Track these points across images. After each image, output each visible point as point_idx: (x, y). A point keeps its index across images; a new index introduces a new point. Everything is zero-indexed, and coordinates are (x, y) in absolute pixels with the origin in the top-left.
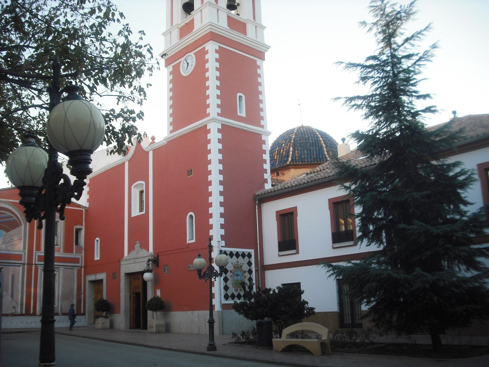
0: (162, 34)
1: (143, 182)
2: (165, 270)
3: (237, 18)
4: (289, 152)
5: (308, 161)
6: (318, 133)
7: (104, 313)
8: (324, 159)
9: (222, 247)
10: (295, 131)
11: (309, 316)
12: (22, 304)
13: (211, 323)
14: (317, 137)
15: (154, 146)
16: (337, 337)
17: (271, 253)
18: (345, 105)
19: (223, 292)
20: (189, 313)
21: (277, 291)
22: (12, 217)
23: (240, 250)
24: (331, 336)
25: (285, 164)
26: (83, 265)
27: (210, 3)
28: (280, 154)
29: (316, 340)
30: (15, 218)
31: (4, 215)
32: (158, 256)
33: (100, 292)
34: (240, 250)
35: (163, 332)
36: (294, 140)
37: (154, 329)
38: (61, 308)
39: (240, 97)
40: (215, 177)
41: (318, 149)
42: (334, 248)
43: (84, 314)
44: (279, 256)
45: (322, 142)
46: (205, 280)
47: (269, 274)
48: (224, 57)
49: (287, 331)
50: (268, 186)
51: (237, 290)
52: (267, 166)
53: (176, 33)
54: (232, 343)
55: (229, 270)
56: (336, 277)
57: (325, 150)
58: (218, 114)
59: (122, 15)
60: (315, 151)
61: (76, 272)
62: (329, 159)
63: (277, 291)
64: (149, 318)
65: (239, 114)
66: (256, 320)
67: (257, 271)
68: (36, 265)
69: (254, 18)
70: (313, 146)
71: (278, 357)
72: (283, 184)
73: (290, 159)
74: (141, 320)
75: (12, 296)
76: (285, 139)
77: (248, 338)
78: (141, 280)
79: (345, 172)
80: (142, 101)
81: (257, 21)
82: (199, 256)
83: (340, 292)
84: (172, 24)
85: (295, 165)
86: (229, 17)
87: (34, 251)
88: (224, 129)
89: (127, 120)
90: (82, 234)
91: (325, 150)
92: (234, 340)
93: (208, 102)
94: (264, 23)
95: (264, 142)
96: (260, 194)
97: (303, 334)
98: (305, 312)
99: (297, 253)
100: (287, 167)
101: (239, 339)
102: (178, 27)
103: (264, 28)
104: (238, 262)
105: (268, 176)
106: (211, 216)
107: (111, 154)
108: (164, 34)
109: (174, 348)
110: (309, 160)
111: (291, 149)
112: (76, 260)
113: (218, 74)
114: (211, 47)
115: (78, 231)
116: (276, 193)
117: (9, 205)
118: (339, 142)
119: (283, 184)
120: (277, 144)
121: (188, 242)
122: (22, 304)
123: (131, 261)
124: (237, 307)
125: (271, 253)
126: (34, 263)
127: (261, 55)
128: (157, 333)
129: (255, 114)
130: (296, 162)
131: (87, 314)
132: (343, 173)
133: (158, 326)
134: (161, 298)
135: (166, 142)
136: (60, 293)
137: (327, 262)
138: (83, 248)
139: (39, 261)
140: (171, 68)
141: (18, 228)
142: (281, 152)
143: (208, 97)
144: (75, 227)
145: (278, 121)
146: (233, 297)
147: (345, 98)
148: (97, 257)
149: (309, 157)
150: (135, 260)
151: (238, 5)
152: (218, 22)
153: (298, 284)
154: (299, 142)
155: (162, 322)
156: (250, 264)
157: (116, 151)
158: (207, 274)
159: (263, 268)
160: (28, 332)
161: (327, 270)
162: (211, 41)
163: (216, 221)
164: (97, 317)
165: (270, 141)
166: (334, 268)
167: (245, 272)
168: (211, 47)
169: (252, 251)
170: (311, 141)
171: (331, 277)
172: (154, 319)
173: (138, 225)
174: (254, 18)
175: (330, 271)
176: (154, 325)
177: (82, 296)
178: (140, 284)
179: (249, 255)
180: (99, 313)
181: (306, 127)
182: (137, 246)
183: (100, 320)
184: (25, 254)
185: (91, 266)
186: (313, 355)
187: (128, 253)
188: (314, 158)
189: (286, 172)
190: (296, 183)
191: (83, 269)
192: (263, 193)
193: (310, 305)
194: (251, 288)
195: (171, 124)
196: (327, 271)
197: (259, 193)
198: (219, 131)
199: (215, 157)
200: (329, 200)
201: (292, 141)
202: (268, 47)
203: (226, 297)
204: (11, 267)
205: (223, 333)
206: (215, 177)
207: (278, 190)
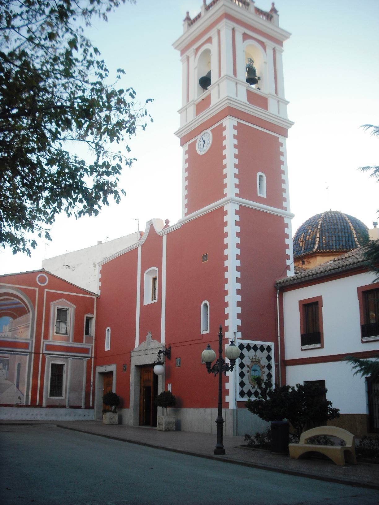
0: (178, 111)
1: (157, 269)
2: (177, 363)
3: (257, 92)
4: (315, 238)
5: (336, 249)
6: (347, 219)
7: (113, 407)
8: (354, 246)
9: (238, 338)
10: (322, 216)
11: (333, 418)
12: (28, 395)
13: (220, 422)
14: (347, 223)
15: (168, 230)
16: (364, 444)
17: (293, 347)
18: (374, 176)
19: (239, 388)
20: (202, 410)
21: (296, 389)
22: (20, 304)
23: (259, 343)
24: (357, 442)
25: (311, 252)
26: (93, 356)
27: (228, 77)
28: (306, 241)
29: (339, 447)
30: (23, 304)
31: (9, 302)
32: (170, 348)
33: (109, 384)
34: (259, 343)
35: (173, 431)
36: (321, 226)
37: (164, 426)
38: (69, 401)
39: (261, 176)
40: (232, 263)
41: (347, 236)
42: (363, 342)
43: (93, 408)
44: (302, 350)
45: (352, 227)
46: (214, 374)
47: (290, 370)
48: (243, 134)
49: (306, 435)
50: (291, 274)
51: (254, 387)
52: (290, 252)
53: (192, 110)
54: (244, 446)
55: (246, 365)
56: (363, 374)
57: (355, 236)
58: (236, 195)
59: (96, 50)
60: (344, 238)
61: (85, 363)
62: (359, 246)
63: (296, 389)
64: (159, 414)
65: (259, 195)
66: (272, 420)
67: (277, 366)
68: (43, 354)
69: (276, 92)
70: (342, 232)
71: (294, 465)
72: (307, 271)
73: (316, 246)
74: (151, 415)
75: (18, 386)
76: (310, 226)
77: (263, 441)
78: (152, 374)
79: (375, 252)
80: (131, 162)
81: (280, 95)
82: (209, 347)
83: (370, 391)
84: (188, 101)
85: (322, 253)
86: (248, 91)
87: (42, 340)
88: (243, 211)
89: (101, 174)
90: (93, 323)
91: (355, 236)
92: (246, 443)
93: (225, 181)
94: (287, 98)
95: (287, 226)
96: (282, 281)
97: (326, 440)
98: (329, 413)
99: (322, 347)
100: (313, 255)
101: (253, 441)
102: (194, 104)
103: (287, 103)
104: (256, 356)
105: (290, 262)
106: (227, 305)
107: (80, 216)
108: (180, 111)
109: (179, 449)
110: (338, 247)
111: (318, 235)
112: (86, 351)
113: (236, 151)
114: (229, 123)
115: (89, 320)
116: (300, 281)
117: (17, 291)
118: (370, 227)
119: (307, 271)
120: (302, 231)
121: (202, 333)
122: (28, 395)
123: (142, 353)
124: (250, 406)
125: (293, 347)
126: (41, 352)
127: (284, 133)
128: (166, 431)
129: (277, 194)
130: (323, 250)
131: (95, 407)
132: (372, 254)
133: (167, 423)
134: (171, 393)
135: (180, 225)
136: (68, 384)
137: (354, 357)
138: (94, 338)
139: (46, 350)
140: (186, 147)
141: (25, 315)
142: (307, 239)
143: (225, 176)
144: (86, 316)
145: (302, 207)
146: (249, 394)
147: (375, 168)
148: (107, 348)
149: (338, 244)
150: (145, 351)
151: (259, 78)
152: (237, 96)
153: (323, 382)
154: (326, 228)
155: (172, 419)
156: (269, 358)
157: (87, 212)
158: (219, 368)
159: (284, 363)
160: (31, 424)
161: (353, 365)
162: (229, 117)
163: (233, 310)
164: (105, 411)
165: (294, 226)
166: (361, 364)
167: (264, 367)
168: (229, 123)
169: (272, 345)
170: (339, 227)
171: (358, 374)
172: (164, 415)
173: (150, 313)
174: (276, 92)
175: (357, 366)
176: (163, 422)
177: (92, 388)
178: (151, 378)
179: (269, 349)
180: (108, 407)
181: (334, 212)
182: (149, 336)
183: (108, 415)
184: (32, 342)
185: (100, 357)
186: (334, 464)
187: (140, 344)
188: (343, 245)
189: (312, 260)
190: (322, 269)
191: (93, 359)
192: (285, 281)
193: (334, 406)
194: (269, 384)
195: (186, 206)
196: (354, 367)
197: (281, 281)
198: (237, 212)
199: (232, 240)
200: (358, 288)
201: (319, 227)
202: (292, 124)
203: (242, 394)
204: (17, 356)
205: (237, 434)
206: (232, 263)
207: (302, 277)
